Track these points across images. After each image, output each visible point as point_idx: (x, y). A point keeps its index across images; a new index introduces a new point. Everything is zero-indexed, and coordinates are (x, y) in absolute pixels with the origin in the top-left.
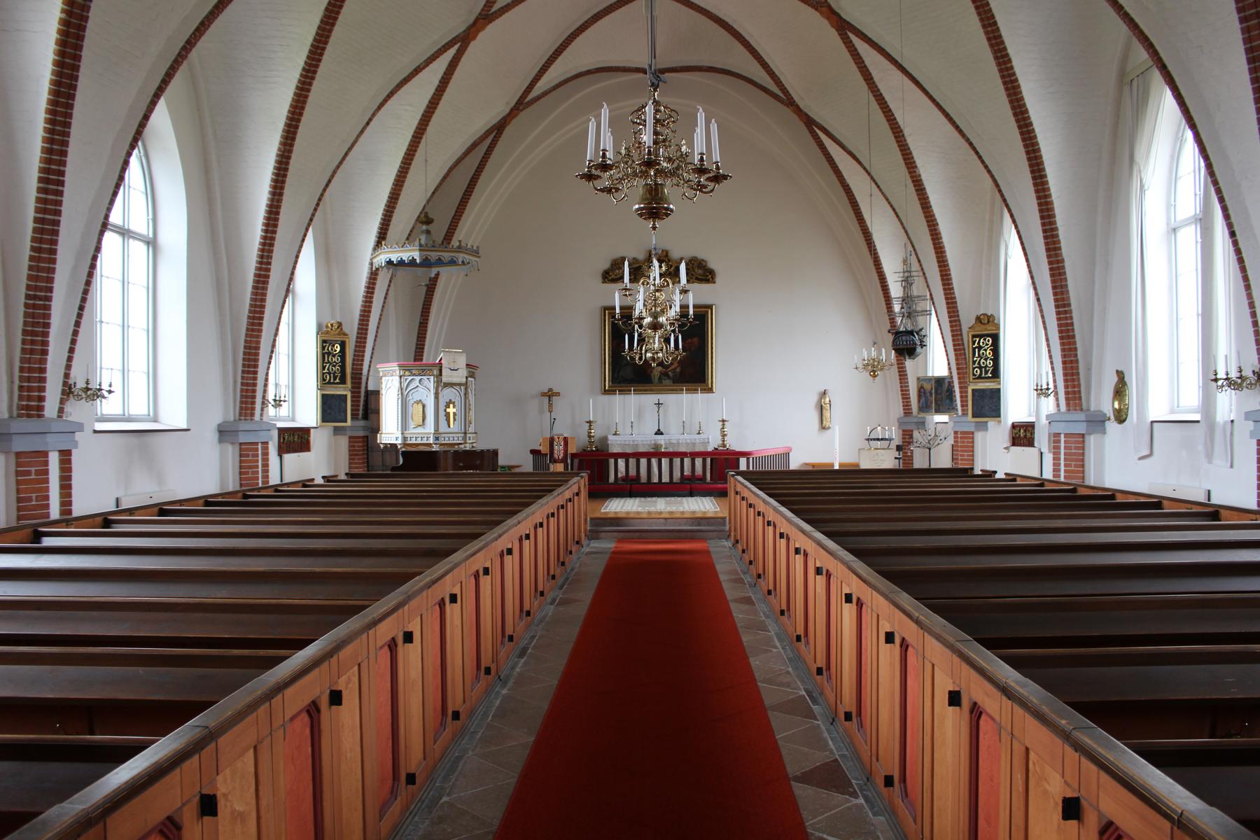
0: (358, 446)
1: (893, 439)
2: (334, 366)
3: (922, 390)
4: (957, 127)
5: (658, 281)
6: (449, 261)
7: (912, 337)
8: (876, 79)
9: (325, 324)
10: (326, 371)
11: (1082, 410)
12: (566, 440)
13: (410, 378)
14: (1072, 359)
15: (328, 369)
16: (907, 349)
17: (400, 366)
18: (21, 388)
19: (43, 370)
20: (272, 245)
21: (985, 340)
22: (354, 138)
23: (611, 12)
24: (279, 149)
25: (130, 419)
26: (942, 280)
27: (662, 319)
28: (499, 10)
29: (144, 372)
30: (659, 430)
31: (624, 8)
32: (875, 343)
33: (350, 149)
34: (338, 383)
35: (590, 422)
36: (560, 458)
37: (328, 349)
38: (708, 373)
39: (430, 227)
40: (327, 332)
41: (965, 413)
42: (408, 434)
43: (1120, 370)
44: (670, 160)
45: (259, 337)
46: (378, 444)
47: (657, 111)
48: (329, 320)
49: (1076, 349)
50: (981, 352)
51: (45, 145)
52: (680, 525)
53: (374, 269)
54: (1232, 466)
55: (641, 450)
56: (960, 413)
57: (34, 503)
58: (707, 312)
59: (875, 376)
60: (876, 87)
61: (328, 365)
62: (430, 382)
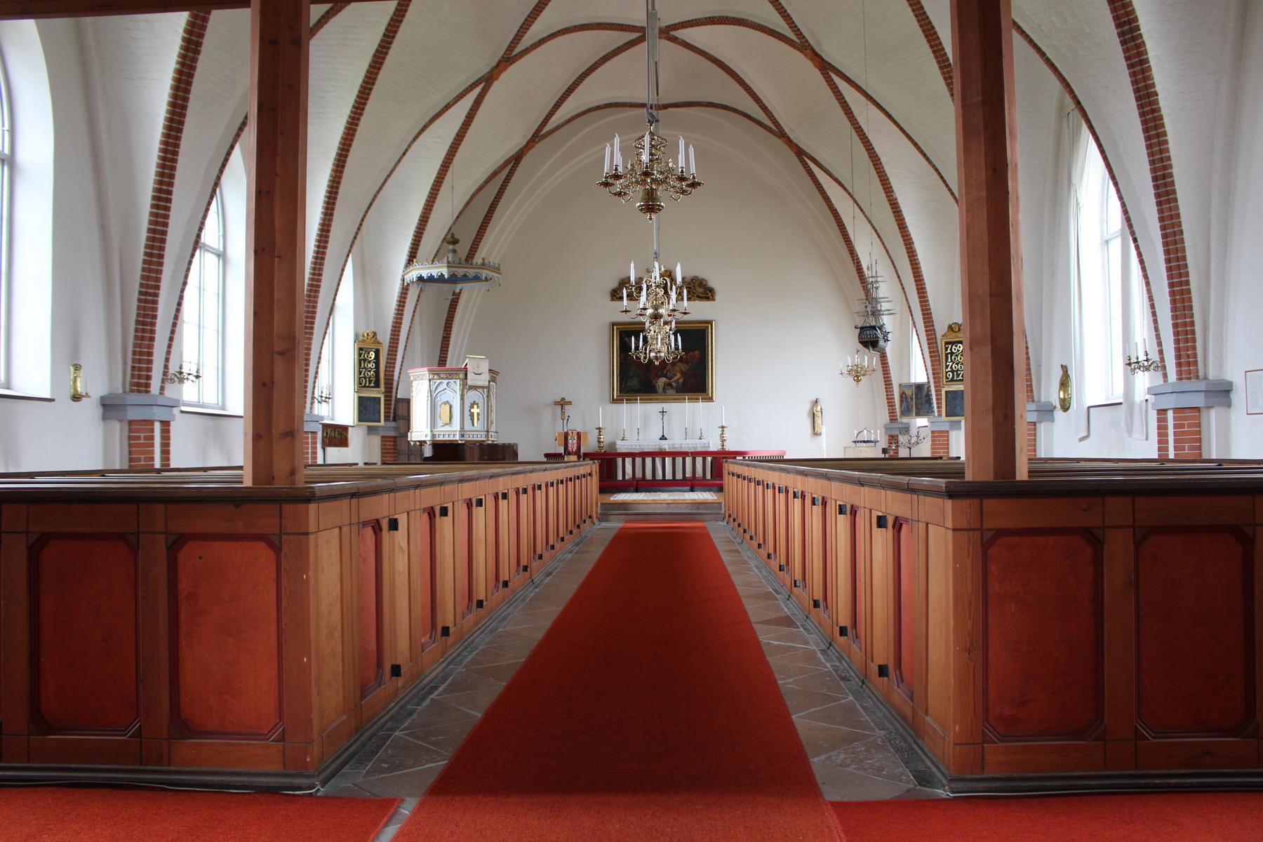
0: (390, 445)
1: (878, 441)
2: (370, 371)
3: (904, 396)
4: (924, 155)
5: (658, 279)
6: (474, 276)
7: (874, 331)
8: (855, 113)
9: (361, 334)
10: (362, 375)
11: (1033, 401)
12: (579, 435)
13: (439, 381)
15: (364, 374)
16: (871, 342)
17: (429, 371)
18: (133, 368)
19: (150, 354)
20: (323, 259)
21: (956, 346)
22: (392, 166)
23: (618, 54)
24: (331, 176)
25: (203, 406)
26: (919, 293)
27: (661, 311)
28: (519, 53)
30: (663, 436)
31: (630, 50)
32: (858, 351)
33: (389, 176)
34: (372, 387)
35: (599, 429)
38: (708, 384)
39: (457, 247)
40: (364, 341)
41: (940, 415)
43: (1064, 364)
44: (662, 173)
45: (310, 339)
46: (409, 442)
47: (652, 139)
48: (364, 330)
50: (953, 358)
51: (158, 170)
52: (680, 509)
53: (405, 284)
54: (1147, 439)
56: (936, 414)
57: (142, 463)
58: (708, 327)
59: (858, 381)
60: (856, 120)
62: (456, 385)
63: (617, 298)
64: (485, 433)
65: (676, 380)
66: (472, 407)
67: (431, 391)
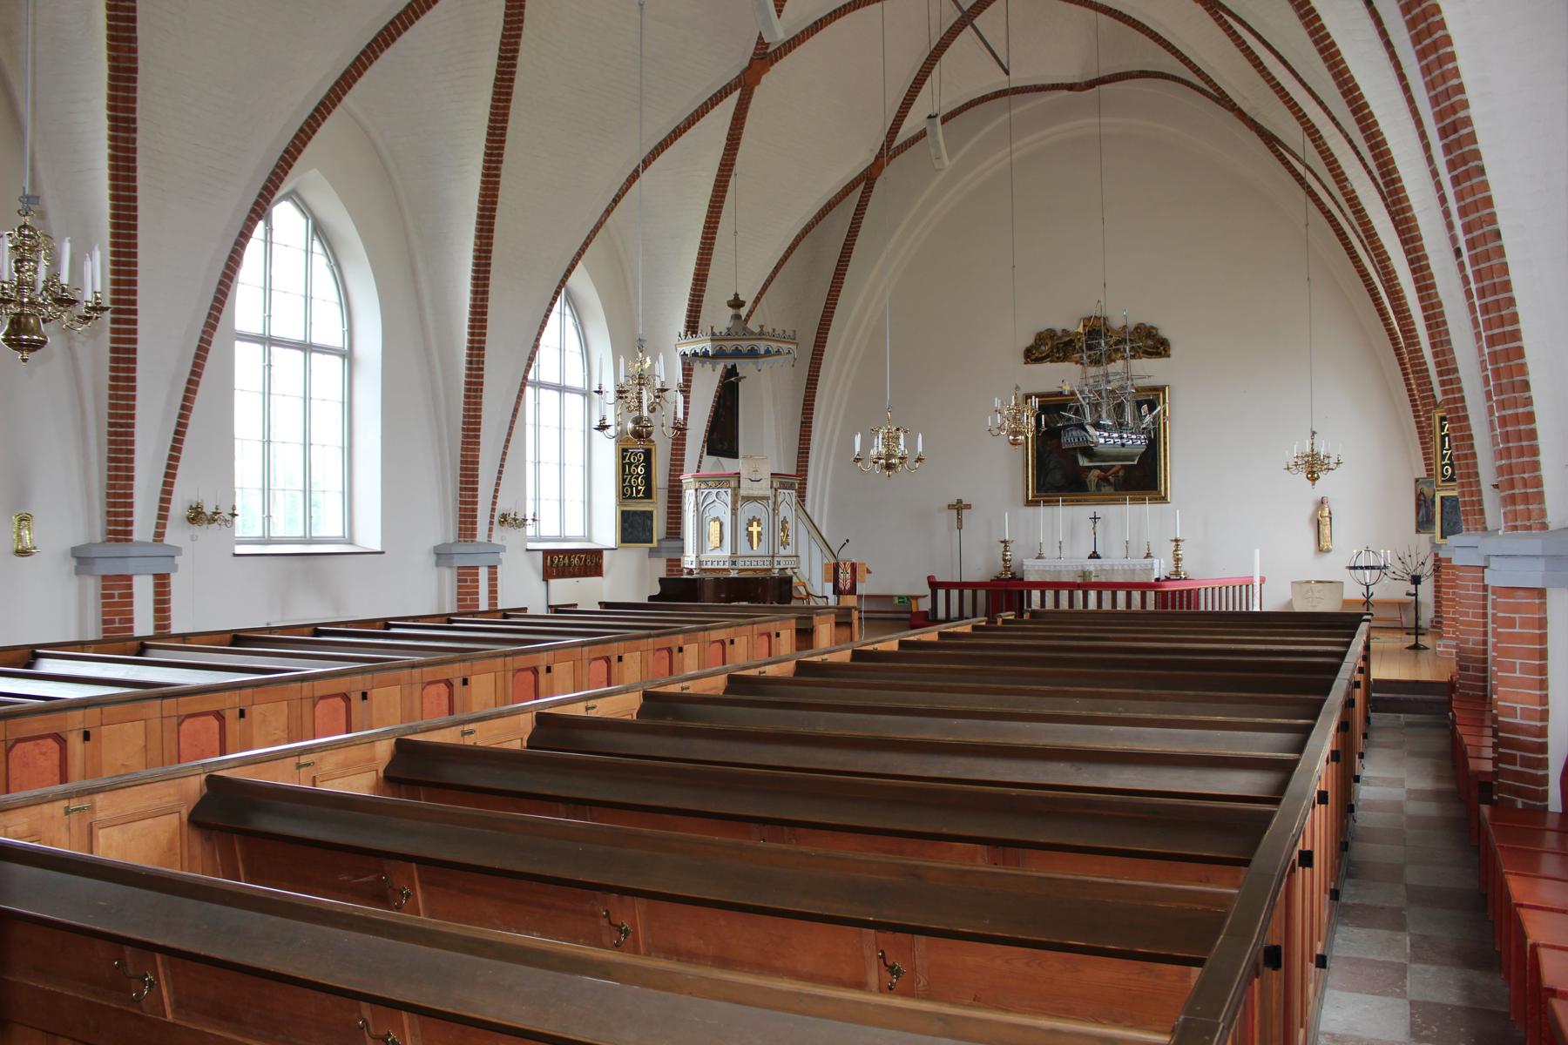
12: (853, 566)
13: (707, 491)
14: (1466, 452)
16: (1080, 448)
25: (566, 540)
30: (1095, 552)
34: (641, 498)
35: (1004, 542)
36: (847, 588)
37: (629, 459)
42: (703, 557)
49: (1471, 437)
55: (1065, 578)
57: (117, 625)
61: (629, 477)
63: (1032, 360)
64: (770, 559)
65: (1114, 473)
67: (697, 504)
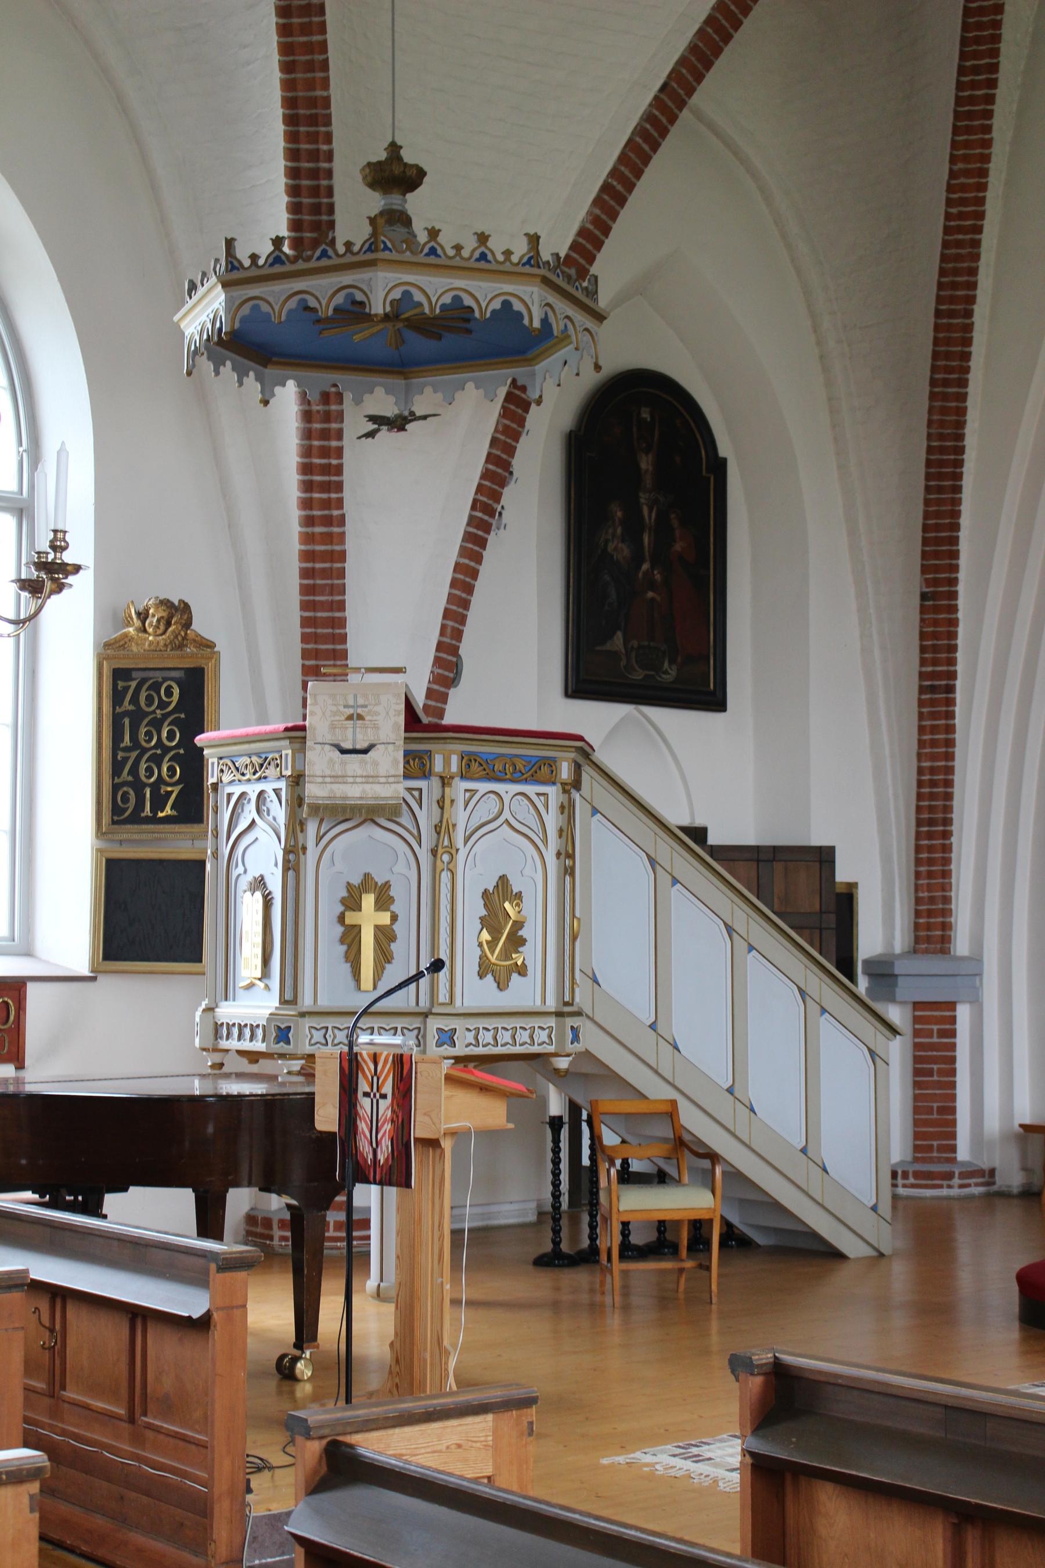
29: (5, 832)
34: (167, 820)
36: (381, 1158)
37: (135, 700)
61: (134, 755)
66: (352, 902)
